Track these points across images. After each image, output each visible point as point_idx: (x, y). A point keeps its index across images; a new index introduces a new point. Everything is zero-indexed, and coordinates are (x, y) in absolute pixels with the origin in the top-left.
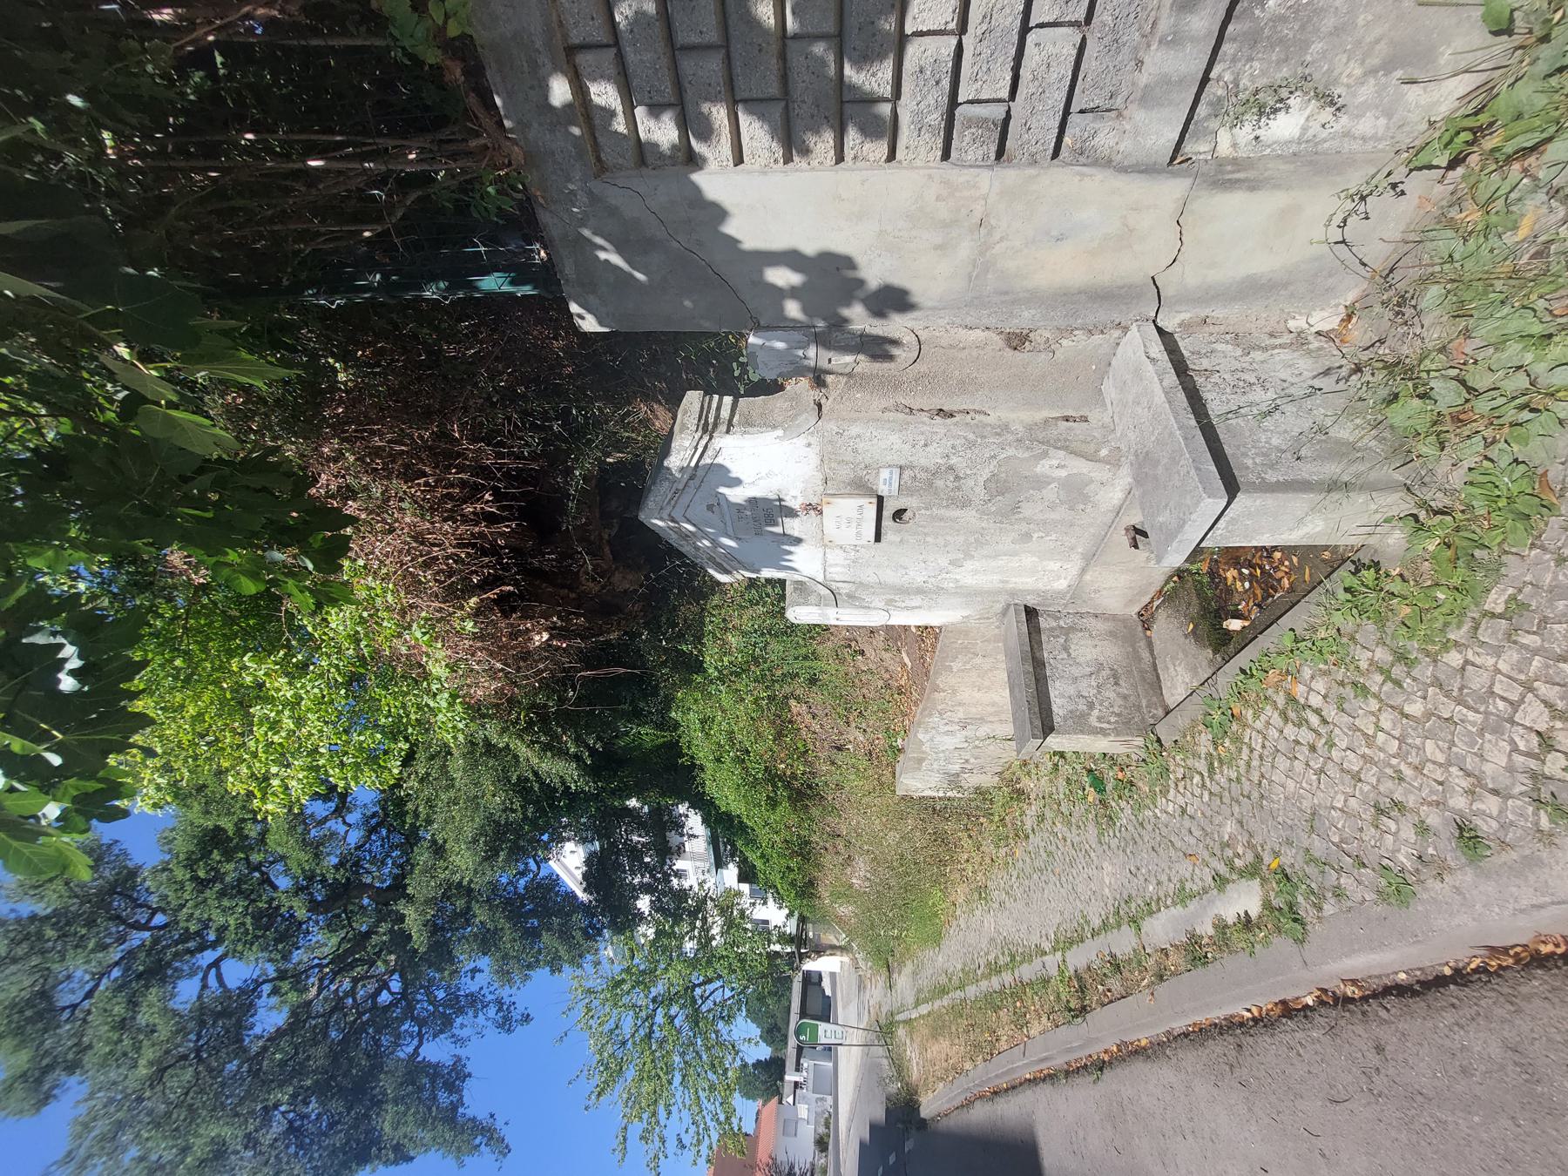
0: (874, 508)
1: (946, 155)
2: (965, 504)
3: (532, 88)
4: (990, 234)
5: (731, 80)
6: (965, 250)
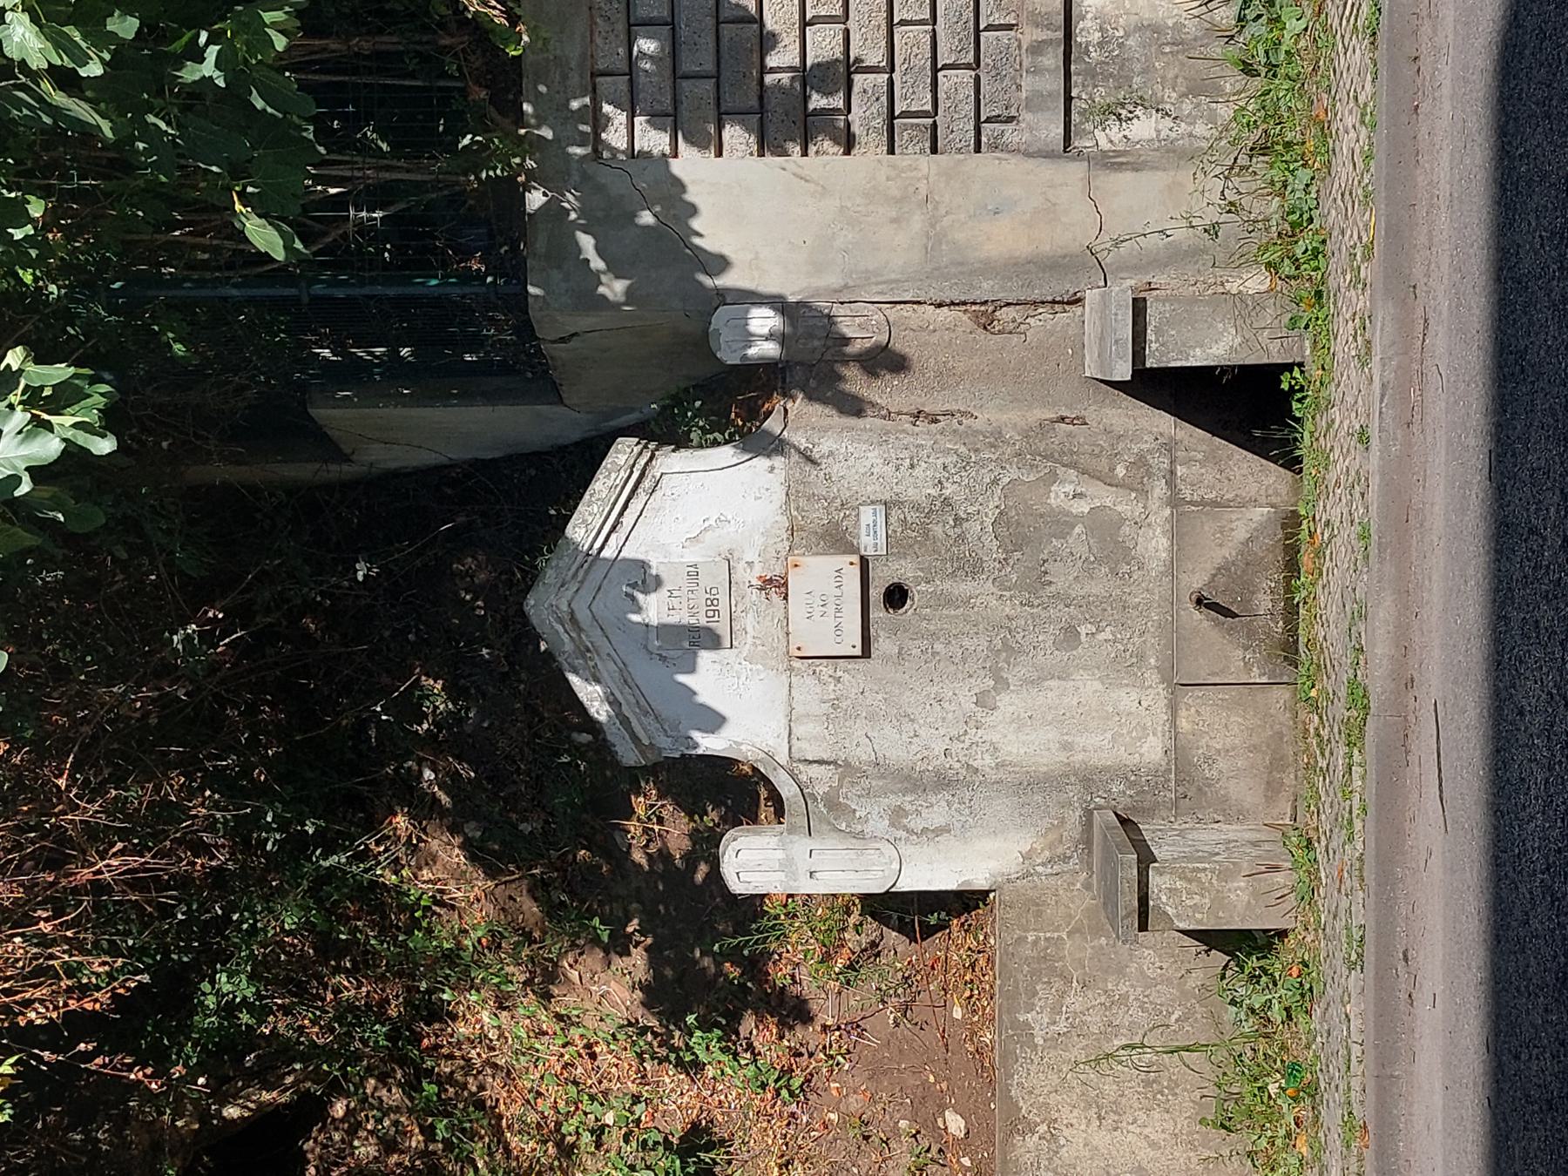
0: (856, 570)
1: (891, 151)
2: (974, 568)
3: (558, 92)
4: (936, 208)
5: (719, 98)
6: (917, 222)
